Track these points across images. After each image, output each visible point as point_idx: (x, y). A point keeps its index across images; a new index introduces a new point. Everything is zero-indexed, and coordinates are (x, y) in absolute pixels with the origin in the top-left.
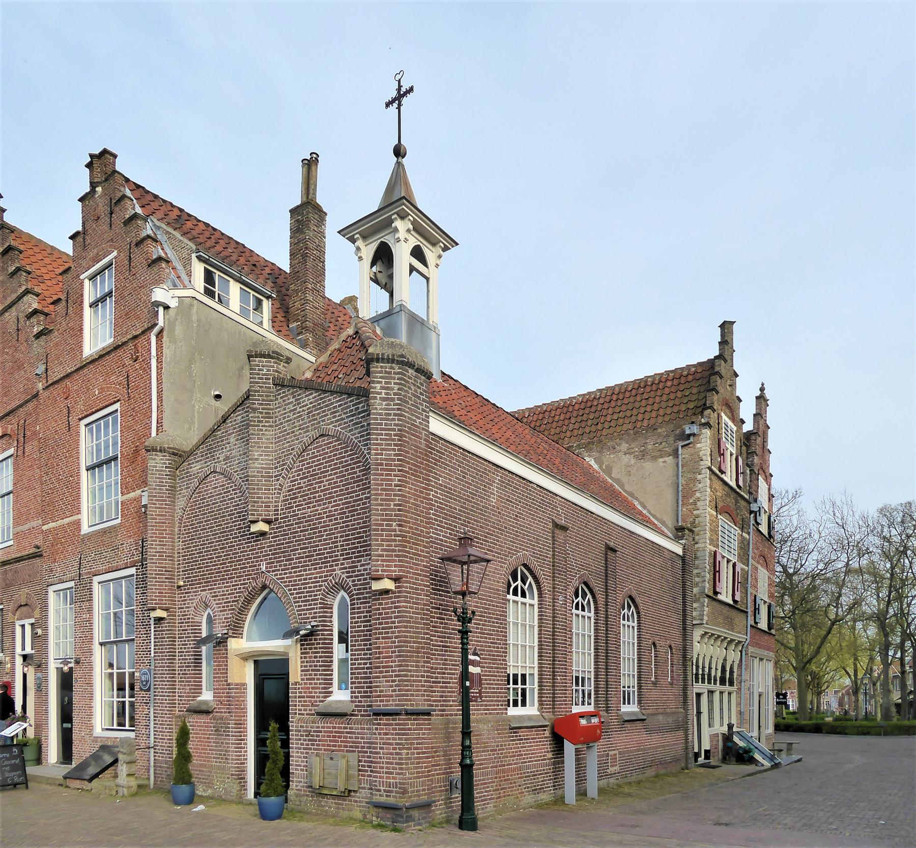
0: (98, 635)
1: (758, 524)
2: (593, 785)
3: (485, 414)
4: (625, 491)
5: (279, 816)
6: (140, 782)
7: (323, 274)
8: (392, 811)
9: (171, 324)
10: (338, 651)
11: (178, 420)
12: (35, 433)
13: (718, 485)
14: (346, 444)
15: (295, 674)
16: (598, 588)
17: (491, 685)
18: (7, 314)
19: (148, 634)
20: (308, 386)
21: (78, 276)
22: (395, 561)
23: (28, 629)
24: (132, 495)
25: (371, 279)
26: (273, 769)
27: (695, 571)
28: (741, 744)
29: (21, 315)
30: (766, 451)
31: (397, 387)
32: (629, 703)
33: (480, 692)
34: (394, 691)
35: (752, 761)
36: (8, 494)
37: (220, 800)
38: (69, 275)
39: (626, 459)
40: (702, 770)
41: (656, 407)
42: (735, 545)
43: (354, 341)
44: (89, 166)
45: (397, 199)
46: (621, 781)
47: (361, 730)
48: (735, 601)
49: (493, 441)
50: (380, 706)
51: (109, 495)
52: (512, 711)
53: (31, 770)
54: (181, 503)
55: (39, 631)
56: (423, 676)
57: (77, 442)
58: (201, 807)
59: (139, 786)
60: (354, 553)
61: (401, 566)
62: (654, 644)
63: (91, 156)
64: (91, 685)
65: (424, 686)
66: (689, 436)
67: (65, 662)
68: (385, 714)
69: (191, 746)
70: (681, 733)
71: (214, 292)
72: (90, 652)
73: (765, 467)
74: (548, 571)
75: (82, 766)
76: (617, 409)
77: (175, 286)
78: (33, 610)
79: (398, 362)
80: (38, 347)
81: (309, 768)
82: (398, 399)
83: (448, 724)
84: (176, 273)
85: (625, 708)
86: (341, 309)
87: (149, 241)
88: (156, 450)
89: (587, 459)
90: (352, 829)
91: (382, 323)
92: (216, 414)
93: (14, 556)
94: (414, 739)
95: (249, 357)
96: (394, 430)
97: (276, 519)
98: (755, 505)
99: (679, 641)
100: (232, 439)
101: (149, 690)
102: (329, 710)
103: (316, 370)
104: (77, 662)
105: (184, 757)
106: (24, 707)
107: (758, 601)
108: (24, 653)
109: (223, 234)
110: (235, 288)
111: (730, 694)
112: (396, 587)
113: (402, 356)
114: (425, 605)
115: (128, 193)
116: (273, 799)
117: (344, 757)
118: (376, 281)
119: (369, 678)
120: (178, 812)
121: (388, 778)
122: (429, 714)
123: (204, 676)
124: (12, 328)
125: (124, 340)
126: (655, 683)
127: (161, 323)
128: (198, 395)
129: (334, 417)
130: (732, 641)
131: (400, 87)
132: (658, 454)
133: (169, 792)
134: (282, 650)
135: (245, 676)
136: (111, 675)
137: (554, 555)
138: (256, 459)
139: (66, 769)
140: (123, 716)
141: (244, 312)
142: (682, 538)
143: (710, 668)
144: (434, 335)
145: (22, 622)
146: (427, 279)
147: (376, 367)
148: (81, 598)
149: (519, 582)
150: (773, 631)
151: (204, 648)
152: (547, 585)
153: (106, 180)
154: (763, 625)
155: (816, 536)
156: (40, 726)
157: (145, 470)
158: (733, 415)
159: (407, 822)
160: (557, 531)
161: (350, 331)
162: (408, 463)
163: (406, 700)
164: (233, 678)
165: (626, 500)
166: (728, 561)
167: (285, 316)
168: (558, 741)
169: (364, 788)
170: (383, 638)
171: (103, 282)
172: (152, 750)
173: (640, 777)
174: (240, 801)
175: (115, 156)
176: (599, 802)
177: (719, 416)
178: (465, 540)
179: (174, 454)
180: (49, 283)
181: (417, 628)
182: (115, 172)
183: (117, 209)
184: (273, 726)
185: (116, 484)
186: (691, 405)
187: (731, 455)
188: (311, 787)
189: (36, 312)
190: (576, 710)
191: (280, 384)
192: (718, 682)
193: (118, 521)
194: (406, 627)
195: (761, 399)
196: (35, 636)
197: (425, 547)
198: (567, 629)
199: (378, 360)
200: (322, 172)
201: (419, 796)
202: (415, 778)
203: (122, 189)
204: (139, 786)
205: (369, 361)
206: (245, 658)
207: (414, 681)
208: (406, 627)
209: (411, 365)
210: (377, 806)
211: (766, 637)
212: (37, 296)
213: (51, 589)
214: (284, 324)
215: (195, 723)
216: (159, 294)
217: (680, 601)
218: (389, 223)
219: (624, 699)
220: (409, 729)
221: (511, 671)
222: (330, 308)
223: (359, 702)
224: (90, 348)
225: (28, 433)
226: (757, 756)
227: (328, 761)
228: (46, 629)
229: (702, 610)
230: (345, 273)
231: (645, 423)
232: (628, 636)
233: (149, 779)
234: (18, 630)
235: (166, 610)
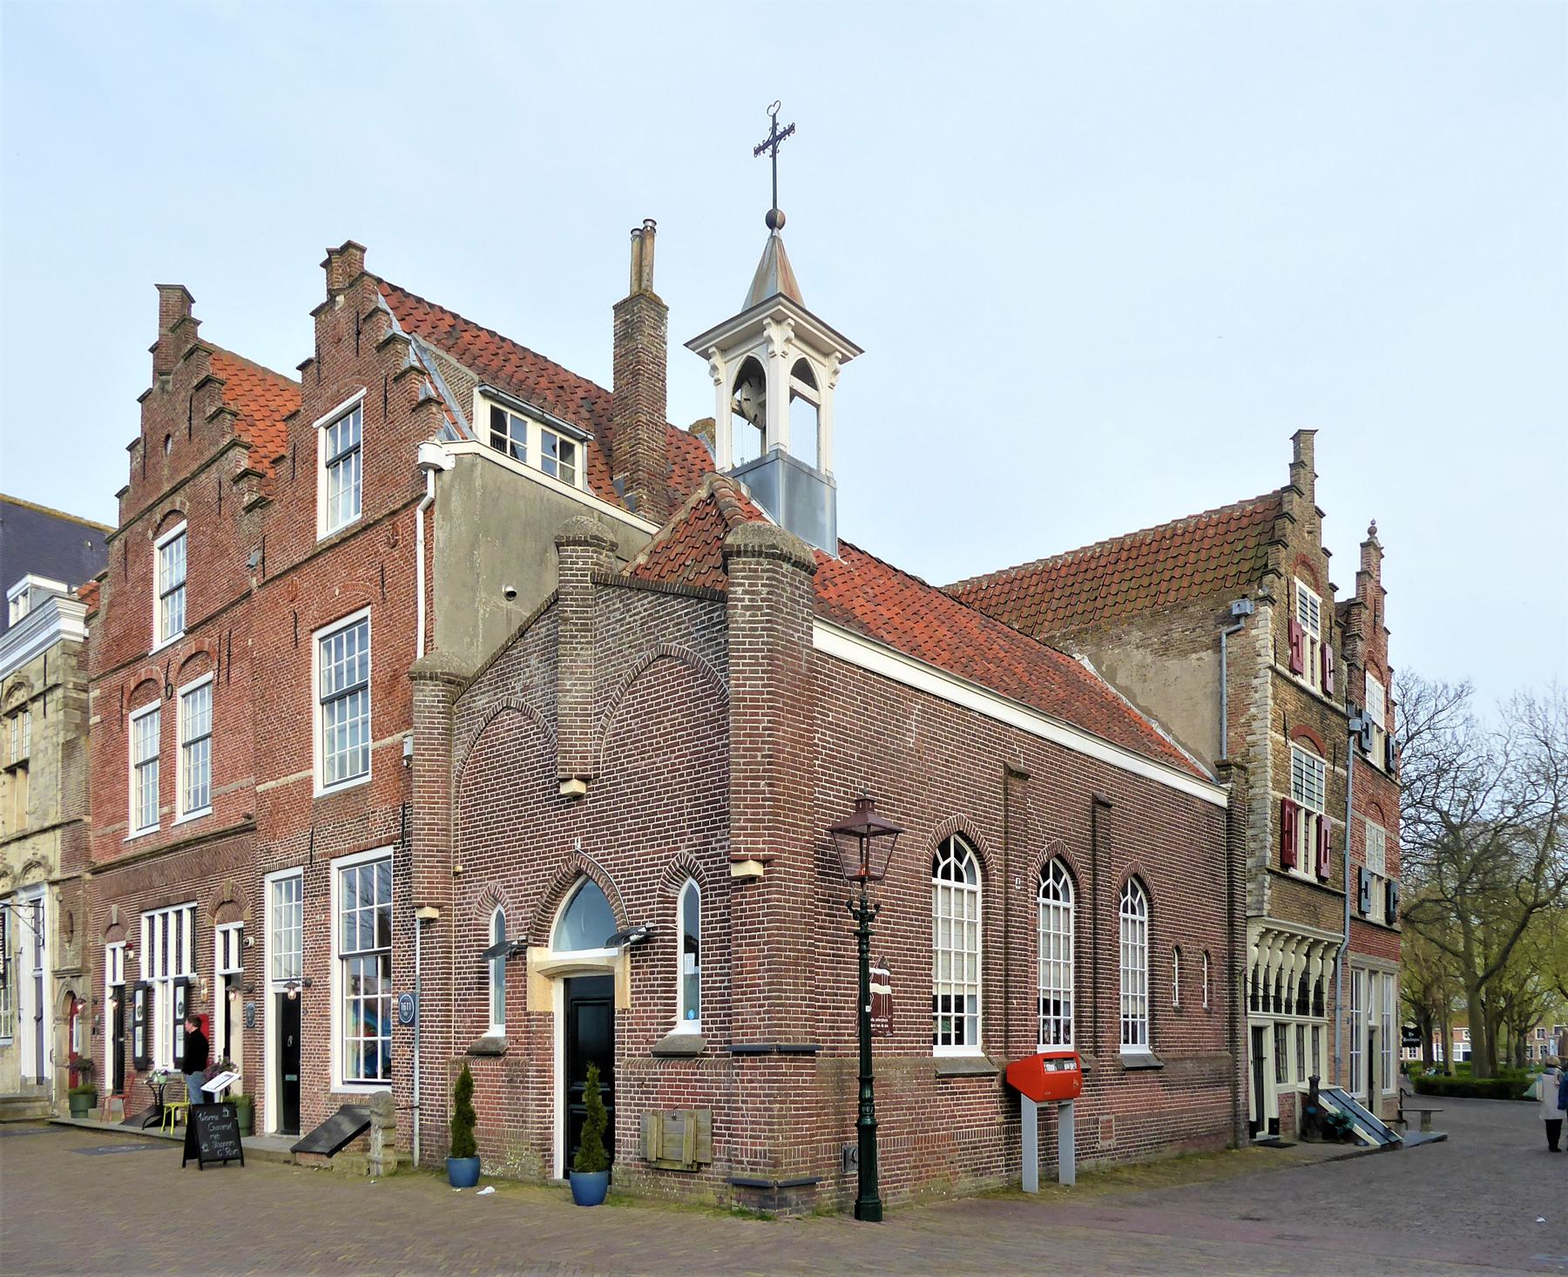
0: (337, 945)
1: (1365, 751)
2: (1067, 1167)
3: (904, 606)
4: (1137, 706)
5: (600, 1201)
6: (402, 1158)
7: (663, 398)
8: (760, 1192)
9: (445, 494)
10: (685, 964)
11: (456, 624)
12: (246, 651)
13: (1287, 693)
14: (696, 669)
15: (623, 997)
16: (1080, 862)
17: (906, 1011)
18: (203, 476)
19: (411, 943)
20: (637, 584)
22: (763, 835)
23: (234, 937)
24: (388, 741)
25: (734, 410)
26: (591, 1132)
27: (1249, 833)
28: (1333, 1109)
29: (226, 479)
30: (1379, 631)
31: (766, 590)
32: (1134, 1041)
33: (890, 1023)
34: (763, 1019)
35: (1350, 1137)
36: (204, 738)
37: (515, 1181)
38: (297, 422)
39: (1138, 655)
40: (1261, 1150)
41: (1189, 569)
42: (1321, 787)
43: (708, 509)
44: (325, 265)
45: (772, 295)
46: (1119, 1162)
47: (713, 1077)
48: (1321, 879)
49: (915, 653)
50: (743, 1040)
51: (354, 741)
52: (940, 1051)
53: (246, 1142)
54: (459, 752)
55: (251, 940)
56: (803, 999)
57: (308, 664)
58: (489, 1190)
59: (399, 1163)
60: (706, 824)
61: (771, 843)
62: (1177, 948)
63: (330, 252)
64: (327, 1017)
65: (804, 1013)
66: (1238, 617)
67: (291, 986)
68: (749, 1053)
69: (474, 1103)
70: (1225, 1091)
71: (504, 441)
72: (326, 970)
73: (1377, 657)
74: (998, 841)
75: (312, 1138)
76: (1128, 575)
77: (450, 438)
78: (241, 909)
79: (768, 556)
80: (251, 524)
81: (641, 1132)
82: (768, 607)
83: (840, 1068)
84: (451, 417)
85: (1126, 1050)
86: (690, 439)
87: (414, 375)
88: (424, 678)
89: (1077, 656)
90: (703, 1217)
91: (750, 477)
92: (509, 620)
93: (213, 830)
94: (791, 1088)
95: (558, 545)
96: (762, 650)
97: (596, 776)
98: (1358, 721)
99: (1223, 943)
100: (533, 662)
101: (412, 1023)
102: (670, 1049)
103: (653, 553)
104: (307, 985)
105: (465, 1118)
106: (227, 1051)
107: (1365, 877)
108: (227, 972)
109: (515, 345)
110: (534, 431)
111: (1316, 1029)
112: (765, 872)
113: (773, 546)
114: (807, 896)
115: (382, 303)
116: (592, 1176)
117: (691, 1115)
118: (741, 413)
119: (727, 1001)
120: (458, 1196)
121: (753, 1144)
122: (812, 1053)
123: (492, 1002)
124: (211, 496)
125: (377, 516)
126: (1178, 1011)
127: (431, 492)
128: (483, 595)
129: (678, 630)
130: (1317, 942)
131: (775, 125)
132: (1189, 647)
133: (442, 1171)
134: (604, 963)
135: (551, 1000)
136: (356, 1003)
137: (1006, 816)
138: (569, 691)
139: (290, 1141)
140: (373, 1062)
141: (547, 467)
142: (1226, 780)
143: (1278, 988)
144: (827, 490)
145: (224, 927)
146: (817, 407)
147: (736, 564)
148: (313, 890)
149: (952, 859)
150: (1397, 926)
151: (492, 962)
152: (995, 862)
153: (351, 285)
154: (1377, 915)
155: (1501, 761)
156: (252, 1080)
157: (408, 705)
158: (1316, 579)
159: (780, 1206)
160: (1012, 780)
161: (703, 493)
162: (782, 696)
163: (779, 1033)
164: (535, 1005)
165: (1137, 721)
166: (1308, 814)
167: (609, 471)
168: (1012, 1098)
169: (719, 1160)
170: (747, 945)
171: (345, 429)
172: (417, 1112)
173: (1152, 1158)
174: (544, 1182)
175: (363, 250)
176: (1077, 1190)
177: (1290, 583)
178: (863, 805)
179: (449, 682)
180: (261, 425)
181: (796, 930)
182: (364, 274)
183: (366, 327)
184: (593, 1071)
185: (365, 723)
186: (1246, 567)
187: (1313, 642)
188: (645, 1159)
189: (246, 474)
190: (1042, 1049)
191: (601, 582)
192: (1294, 1009)
193: (368, 779)
194: (779, 929)
195: (1371, 548)
196: (243, 946)
197: (807, 813)
198: (1030, 927)
199: (739, 554)
200: (661, 246)
201: (797, 1170)
202: (791, 1144)
203: (373, 297)
204: (399, 1163)
205: (727, 555)
206: (551, 975)
207: (791, 1006)
208: (779, 929)
209: (786, 558)
210: (738, 1184)
211: (1383, 936)
212: (247, 448)
213: (269, 878)
214: (606, 476)
215: (478, 1067)
216: (430, 453)
217: (1224, 880)
218: (759, 329)
219: (1126, 1032)
220: (784, 1074)
221: (940, 992)
222: (674, 440)
223: (715, 1036)
224: (326, 529)
225: (235, 650)
226: (1359, 1130)
227: (669, 1122)
228: (260, 937)
229: (1262, 894)
230: (693, 392)
231: (1172, 596)
232: (1133, 938)
233: (412, 1153)
234: (109, 955)
235: (439, 907)
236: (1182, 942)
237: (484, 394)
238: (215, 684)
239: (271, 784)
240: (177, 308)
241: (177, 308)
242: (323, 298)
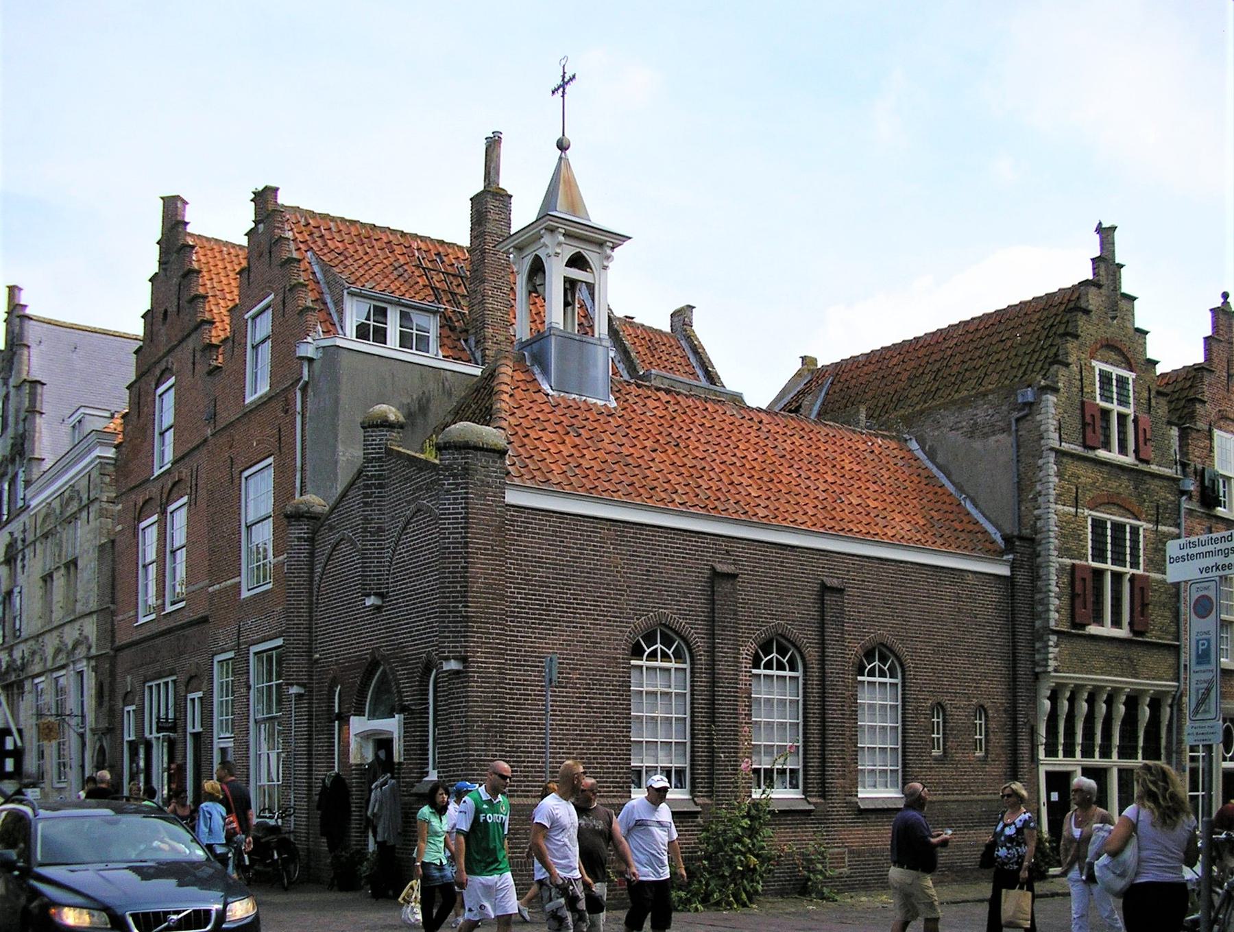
21: (243, 314)
74: (702, 627)
200: (505, 150)
238: (189, 504)
240: (173, 210)
241: (173, 210)
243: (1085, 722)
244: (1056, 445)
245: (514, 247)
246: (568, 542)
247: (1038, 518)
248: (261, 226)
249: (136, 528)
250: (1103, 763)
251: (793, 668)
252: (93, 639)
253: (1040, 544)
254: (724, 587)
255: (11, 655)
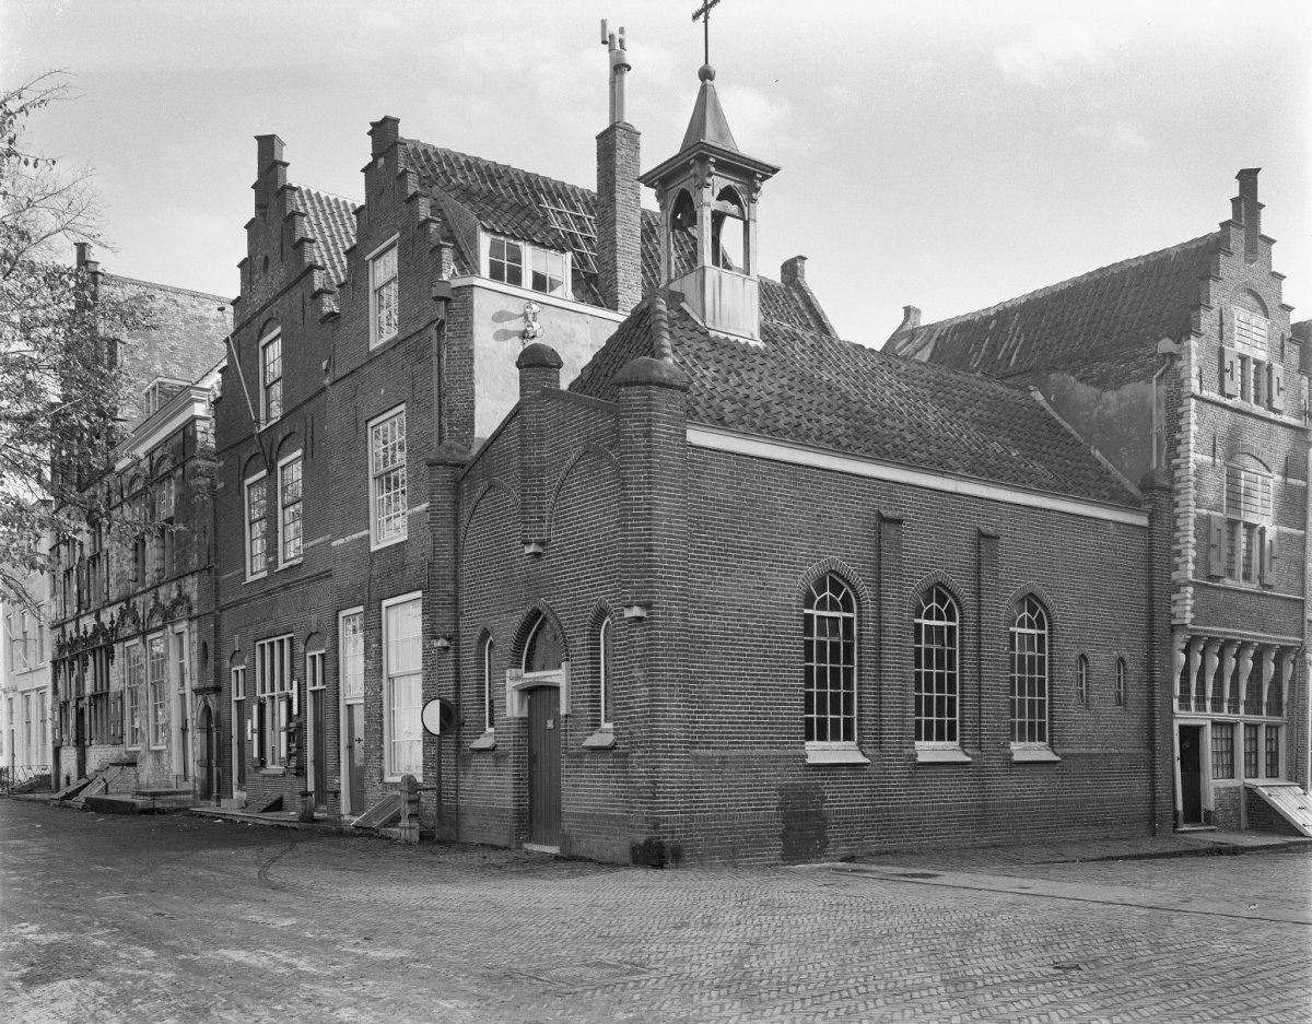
108: (316, 688)
112: (648, 614)
192: (1208, 704)
234: (233, 676)
236: (1087, 651)
237: (485, 230)
238: (304, 457)
239: (341, 541)
242: (370, 159)
243: (1198, 676)
244: (1197, 392)
245: (696, 158)
246: (745, 485)
247: (1178, 467)
248: (381, 161)
249: (241, 484)
250: (1232, 718)
251: (951, 618)
252: (194, 597)
253: (1178, 494)
254: (890, 532)
255: (98, 618)
